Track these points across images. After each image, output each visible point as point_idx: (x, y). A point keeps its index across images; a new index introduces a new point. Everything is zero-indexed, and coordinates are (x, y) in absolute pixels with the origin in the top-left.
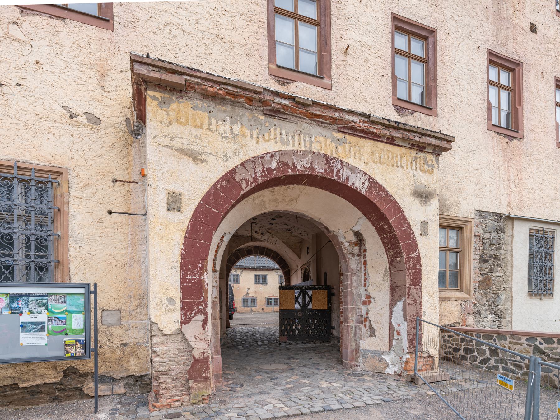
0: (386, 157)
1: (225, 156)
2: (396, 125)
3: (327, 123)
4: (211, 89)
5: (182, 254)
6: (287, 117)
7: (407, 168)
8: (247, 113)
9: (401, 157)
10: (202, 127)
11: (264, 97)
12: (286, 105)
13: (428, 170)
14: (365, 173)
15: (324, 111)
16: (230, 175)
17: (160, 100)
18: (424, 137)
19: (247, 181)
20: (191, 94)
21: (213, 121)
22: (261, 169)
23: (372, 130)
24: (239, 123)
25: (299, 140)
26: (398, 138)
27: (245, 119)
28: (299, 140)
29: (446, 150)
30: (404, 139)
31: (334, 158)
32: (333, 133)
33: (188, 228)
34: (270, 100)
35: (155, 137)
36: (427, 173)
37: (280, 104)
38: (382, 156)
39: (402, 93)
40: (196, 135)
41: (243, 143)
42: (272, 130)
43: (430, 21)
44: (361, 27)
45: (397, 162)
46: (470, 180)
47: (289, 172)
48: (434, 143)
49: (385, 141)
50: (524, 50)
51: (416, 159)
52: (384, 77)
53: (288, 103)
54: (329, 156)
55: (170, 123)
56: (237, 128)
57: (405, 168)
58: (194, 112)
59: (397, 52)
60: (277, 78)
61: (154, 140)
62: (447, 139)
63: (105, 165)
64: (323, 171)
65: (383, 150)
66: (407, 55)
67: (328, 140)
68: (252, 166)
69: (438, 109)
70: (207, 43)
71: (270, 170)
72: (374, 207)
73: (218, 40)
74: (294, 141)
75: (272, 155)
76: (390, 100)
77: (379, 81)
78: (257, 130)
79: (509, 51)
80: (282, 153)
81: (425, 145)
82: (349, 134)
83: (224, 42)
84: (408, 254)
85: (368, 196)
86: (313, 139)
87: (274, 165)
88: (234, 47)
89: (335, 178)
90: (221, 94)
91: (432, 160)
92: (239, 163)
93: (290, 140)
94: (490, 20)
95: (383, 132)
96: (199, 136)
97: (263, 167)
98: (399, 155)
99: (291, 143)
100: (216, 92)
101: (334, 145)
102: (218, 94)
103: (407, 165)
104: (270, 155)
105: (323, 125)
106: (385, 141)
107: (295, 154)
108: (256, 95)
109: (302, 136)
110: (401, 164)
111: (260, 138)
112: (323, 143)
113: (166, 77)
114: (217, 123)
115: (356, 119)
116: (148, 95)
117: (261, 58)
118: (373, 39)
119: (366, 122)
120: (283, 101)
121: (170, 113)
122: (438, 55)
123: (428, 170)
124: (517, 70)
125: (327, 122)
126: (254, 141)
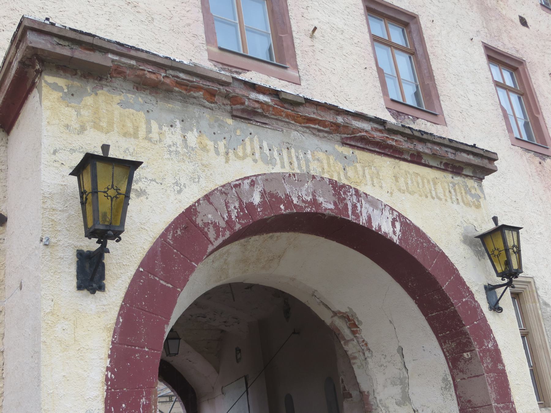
0: (415, 183)
1: (176, 183)
2: (421, 136)
3: (326, 132)
4: (153, 77)
5: (107, 379)
6: (267, 121)
7: (446, 200)
8: (207, 114)
9: (435, 184)
10: (135, 136)
11: (234, 91)
12: (266, 103)
13: (474, 202)
14: (392, 209)
15: (322, 114)
16: (188, 217)
17: (66, 90)
18: (458, 153)
19: (216, 226)
20: (118, 82)
21: (154, 126)
22: (237, 205)
23: (390, 142)
24: (195, 130)
25: (290, 157)
26: (426, 154)
27: (204, 123)
28: (290, 157)
29: (490, 171)
30: (434, 156)
31: (344, 186)
32: (337, 146)
33: (117, 323)
34: (244, 96)
35: (55, 152)
36: (473, 208)
37: (257, 102)
38: (409, 182)
39: (394, 94)
40: (127, 149)
41: (204, 162)
42: (247, 141)
43: (408, 4)
44: (326, 6)
45: (430, 190)
46: (512, 217)
47: (281, 209)
48: (473, 162)
49: (409, 159)
50: (522, 46)
51: (454, 186)
52: (368, 70)
53: (269, 101)
54: (336, 181)
55: (83, 129)
56: (192, 137)
57: (444, 200)
58: (122, 110)
59: (375, 39)
60: (221, 66)
61: (54, 157)
62: (489, 156)
63: (426, 184)
64: (332, 206)
65: (409, 172)
66: (388, 44)
67: (331, 157)
68: (222, 201)
69: (445, 115)
70: (112, 11)
71: (250, 206)
72: (410, 265)
73: (129, 8)
74: (282, 159)
75: (252, 181)
76: (382, 101)
77: (362, 74)
78: (224, 141)
79: (506, 46)
80: (268, 178)
81: (462, 166)
82: (358, 148)
83: (138, 12)
84: (481, 344)
85: (403, 246)
86: (309, 156)
87: (256, 199)
88: (153, 19)
89: (351, 218)
90: (167, 85)
91: (474, 187)
92: (200, 195)
93: (275, 156)
94: (475, 8)
95: (405, 145)
96: (131, 150)
97: (241, 201)
98: (431, 180)
99: (278, 161)
100: (160, 81)
101: (340, 166)
102: (163, 83)
103: (445, 195)
104: (249, 181)
105: (321, 134)
106: (409, 159)
107: (286, 179)
108: (221, 87)
109: (293, 150)
110: (436, 193)
111: (230, 154)
112: (325, 162)
113: (80, 54)
114: (161, 128)
115: (366, 126)
116: (46, 82)
117: (195, 36)
118: (344, 21)
119: (380, 131)
120: (262, 98)
121: (83, 112)
122: (427, 46)
123: (474, 202)
124: (520, 69)
125: (326, 129)
126: (222, 159)
